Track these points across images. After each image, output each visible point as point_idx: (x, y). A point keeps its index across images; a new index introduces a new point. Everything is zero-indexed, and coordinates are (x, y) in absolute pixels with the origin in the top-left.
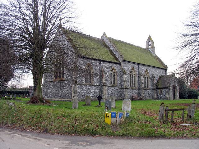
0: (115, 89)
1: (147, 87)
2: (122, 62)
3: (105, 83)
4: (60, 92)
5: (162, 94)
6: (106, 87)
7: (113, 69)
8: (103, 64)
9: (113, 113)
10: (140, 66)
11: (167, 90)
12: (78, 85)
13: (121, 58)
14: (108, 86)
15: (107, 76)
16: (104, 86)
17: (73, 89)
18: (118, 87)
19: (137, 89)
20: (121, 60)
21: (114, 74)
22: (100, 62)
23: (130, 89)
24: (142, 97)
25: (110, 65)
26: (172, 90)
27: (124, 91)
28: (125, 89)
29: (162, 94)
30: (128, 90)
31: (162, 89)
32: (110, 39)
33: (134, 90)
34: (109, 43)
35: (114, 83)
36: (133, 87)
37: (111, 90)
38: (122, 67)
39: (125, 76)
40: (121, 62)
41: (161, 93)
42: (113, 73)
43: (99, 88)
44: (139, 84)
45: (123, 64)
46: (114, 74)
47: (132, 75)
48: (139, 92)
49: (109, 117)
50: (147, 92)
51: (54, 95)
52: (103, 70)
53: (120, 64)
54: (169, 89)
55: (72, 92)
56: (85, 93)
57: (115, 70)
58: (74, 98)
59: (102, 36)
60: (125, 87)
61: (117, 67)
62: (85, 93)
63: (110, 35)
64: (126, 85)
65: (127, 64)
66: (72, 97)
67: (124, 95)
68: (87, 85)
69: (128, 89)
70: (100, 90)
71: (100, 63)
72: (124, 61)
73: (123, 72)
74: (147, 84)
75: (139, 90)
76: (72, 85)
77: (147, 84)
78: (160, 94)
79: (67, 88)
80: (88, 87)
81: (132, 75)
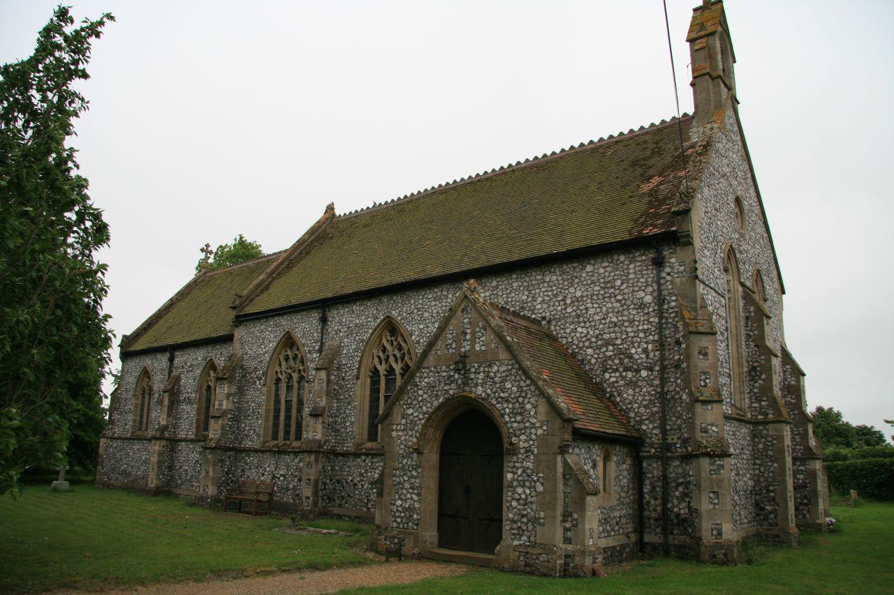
33: (288, 458)
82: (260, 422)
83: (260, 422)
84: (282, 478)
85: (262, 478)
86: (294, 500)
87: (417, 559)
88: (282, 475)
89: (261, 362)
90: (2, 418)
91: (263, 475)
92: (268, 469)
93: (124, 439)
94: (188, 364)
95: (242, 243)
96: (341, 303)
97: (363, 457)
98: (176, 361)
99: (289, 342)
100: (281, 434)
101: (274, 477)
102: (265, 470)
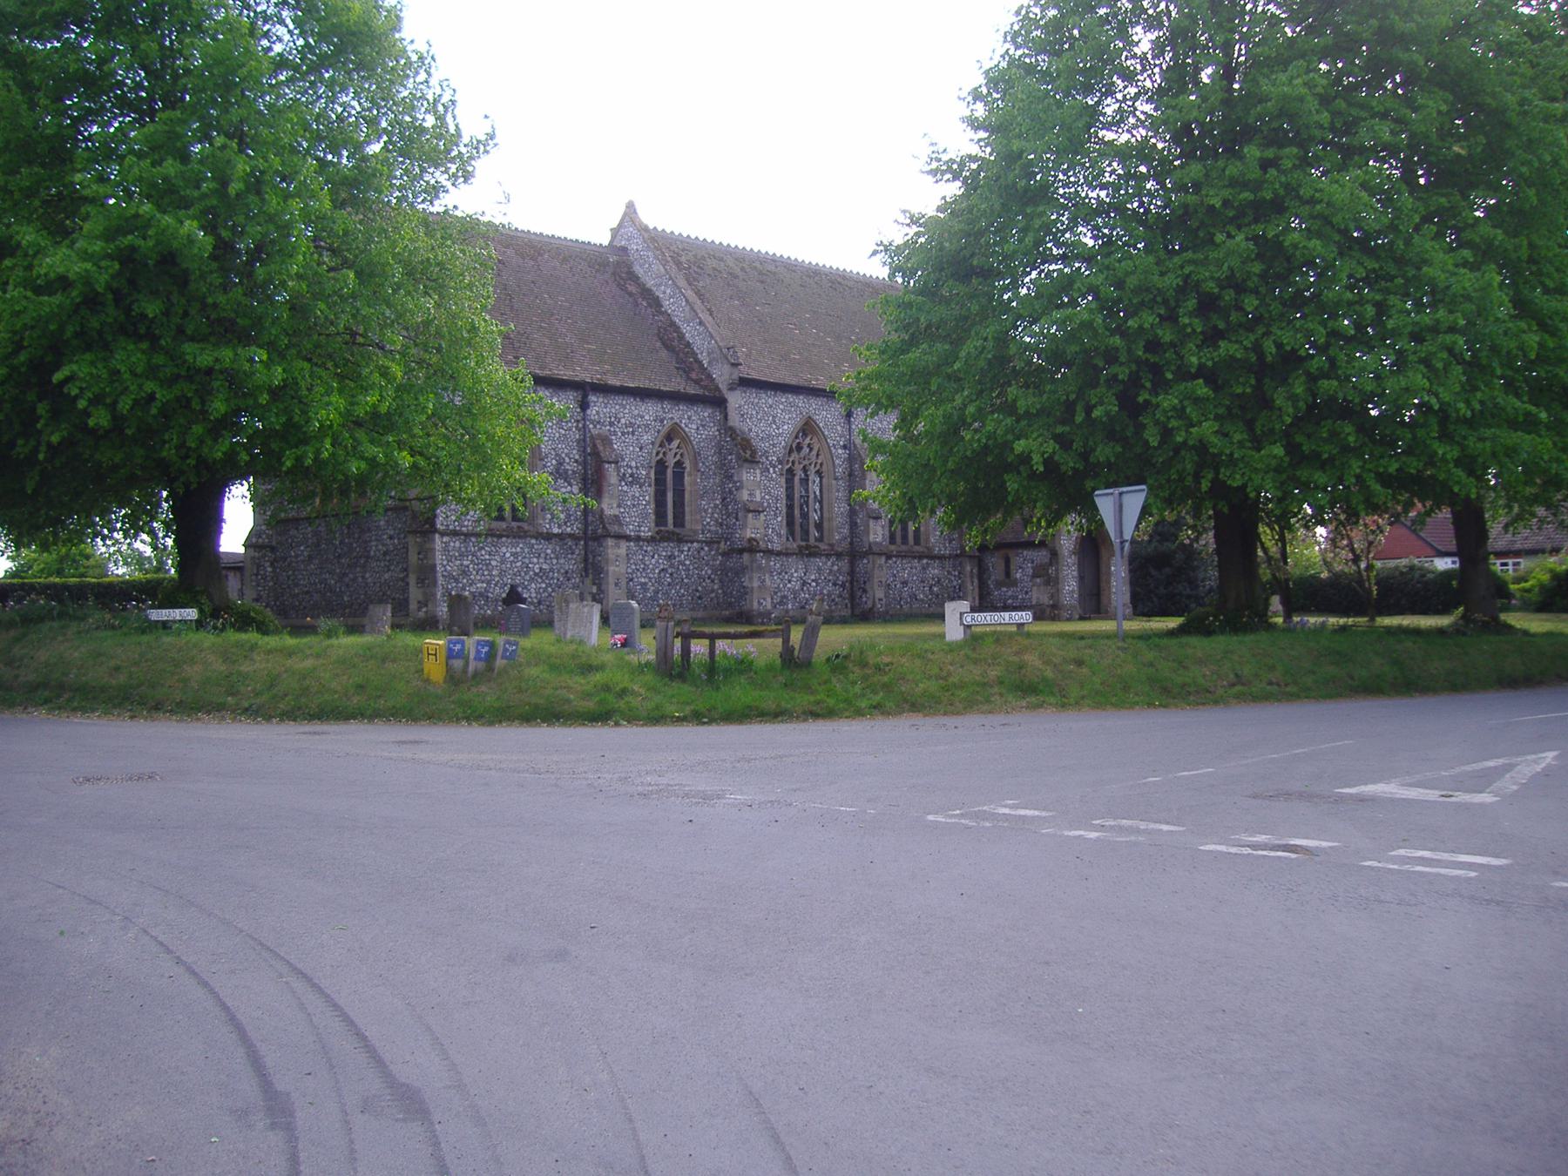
0: (684, 554)
1: (899, 540)
2: (731, 388)
3: (616, 519)
4: (347, 580)
5: (1014, 583)
6: (624, 544)
7: (669, 438)
8: (599, 407)
9: (455, 644)
10: (592, 398)
11: (1041, 556)
12: (443, 534)
13: (727, 367)
14: (638, 539)
15: (635, 480)
16: (610, 542)
17: (413, 558)
18: (709, 543)
19: (839, 555)
20: (721, 375)
21: (679, 464)
22: (585, 396)
23: (787, 555)
24: (870, 604)
25: (649, 411)
26: (1072, 560)
27: (743, 570)
28: (746, 556)
29: (1014, 583)
30: (776, 564)
31: (1011, 553)
32: (661, 243)
33: (819, 562)
34: (658, 268)
35: (679, 520)
36: (812, 541)
37: (656, 559)
38: (734, 420)
39: (749, 476)
40: (723, 387)
41: (1008, 574)
42: (671, 461)
43: (579, 550)
44: (853, 525)
45: (735, 400)
46: (679, 464)
47: (805, 469)
48: (852, 573)
49: (435, 655)
50: (907, 570)
51: (316, 597)
52: (607, 441)
53: (719, 403)
54: (1054, 554)
55: (412, 580)
56: (489, 583)
57: (686, 439)
58: (419, 609)
59: (615, 225)
60: (751, 540)
61: (696, 423)
62: (489, 583)
63: (661, 217)
64: (752, 529)
65: (766, 399)
66: (413, 606)
67: (745, 592)
68: (500, 536)
69: (769, 553)
70: (586, 560)
71: (584, 406)
72: (746, 383)
73: (741, 450)
74: (670, 496)
75: (852, 564)
76: (411, 539)
77: (670, 496)
78: (999, 585)
79: (385, 554)
80: (507, 550)
81: (805, 469)
82: (779, 519)
83: (779, 519)
84: (814, 584)
85: (789, 585)
86: (830, 606)
87: (482, 627)
88: (813, 581)
89: (774, 445)
90: (1260, 525)
91: (790, 582)
92: (795, 575)
93: (467, 535)
94: (623, 421)
95: (611, 230)
96: (772, 389)
97: (894, 559)
98: (592, 412)
99: (808, 428)
100: (899, 540)
101: (804, 583)
102: (792, 575)
